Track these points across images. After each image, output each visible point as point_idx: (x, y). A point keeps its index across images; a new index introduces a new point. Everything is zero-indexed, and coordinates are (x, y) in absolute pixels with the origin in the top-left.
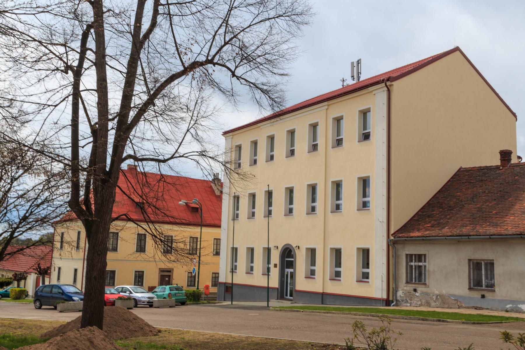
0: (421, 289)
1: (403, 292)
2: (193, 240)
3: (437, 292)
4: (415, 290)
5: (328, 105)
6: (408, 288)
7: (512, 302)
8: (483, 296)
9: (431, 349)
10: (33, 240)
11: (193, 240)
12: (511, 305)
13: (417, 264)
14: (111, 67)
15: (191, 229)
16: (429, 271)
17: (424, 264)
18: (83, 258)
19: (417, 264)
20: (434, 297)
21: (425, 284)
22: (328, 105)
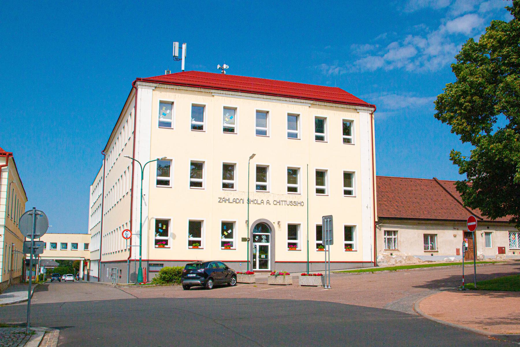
0: (395, 254)
1: (383, 256)
2: (140, 265)
3: (406, 255)
4: (391, 254)
5: (156, 87)
6: (386, 253)
7: (446, 257)
8: (432, 255)
9: (1, 236)
10: (21, 275)
11: (140, 265)
12: (446, 258)
13: (388, 237)
14: (129, 157)
15: (13, 296)
16: (400, 241)
17: (385, 237)
18: (150, 259)
19: (388, 237)
20: (405, 258)
21: (398, 250)
22: (156, 87)
